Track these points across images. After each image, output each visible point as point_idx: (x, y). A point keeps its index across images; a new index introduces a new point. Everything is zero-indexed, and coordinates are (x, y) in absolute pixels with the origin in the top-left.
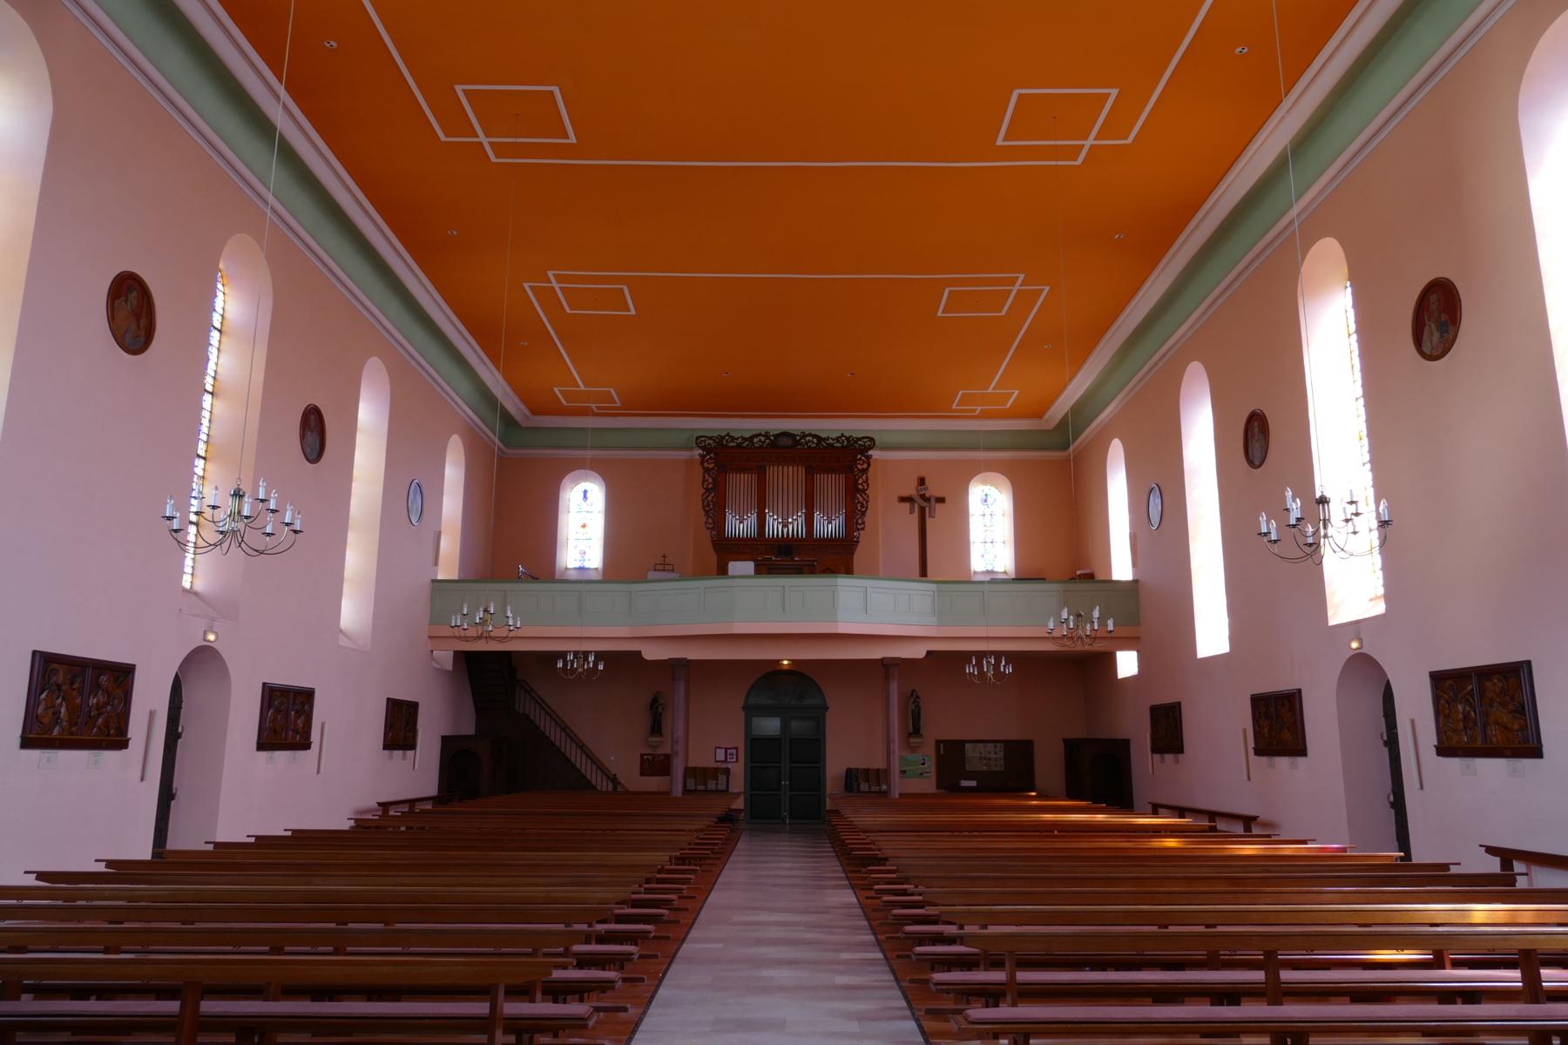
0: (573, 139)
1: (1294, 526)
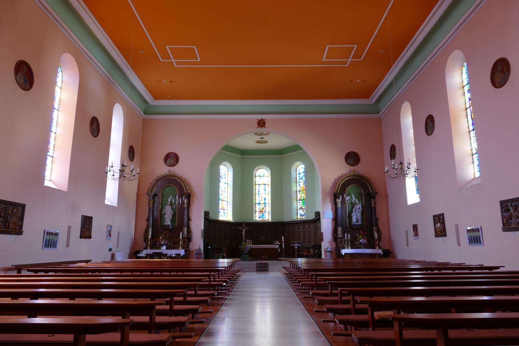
0: (199, 60)
1: (386, 172)
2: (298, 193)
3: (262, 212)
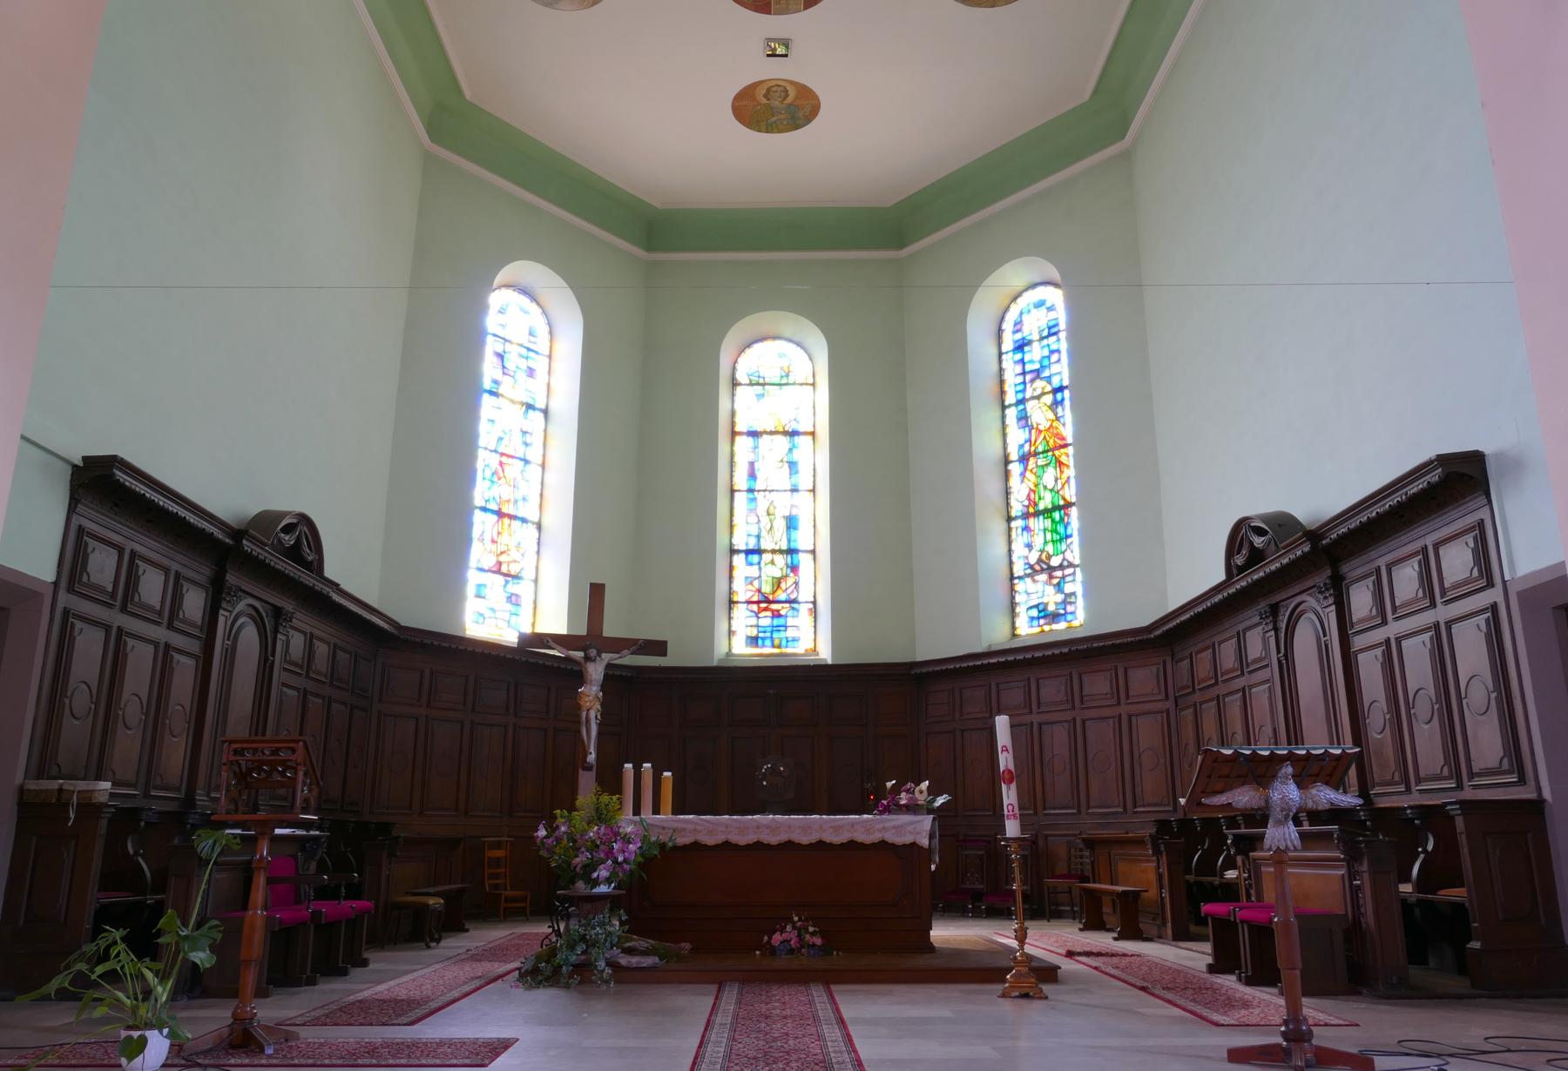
2: (1016, 468)
3: (774, 606)
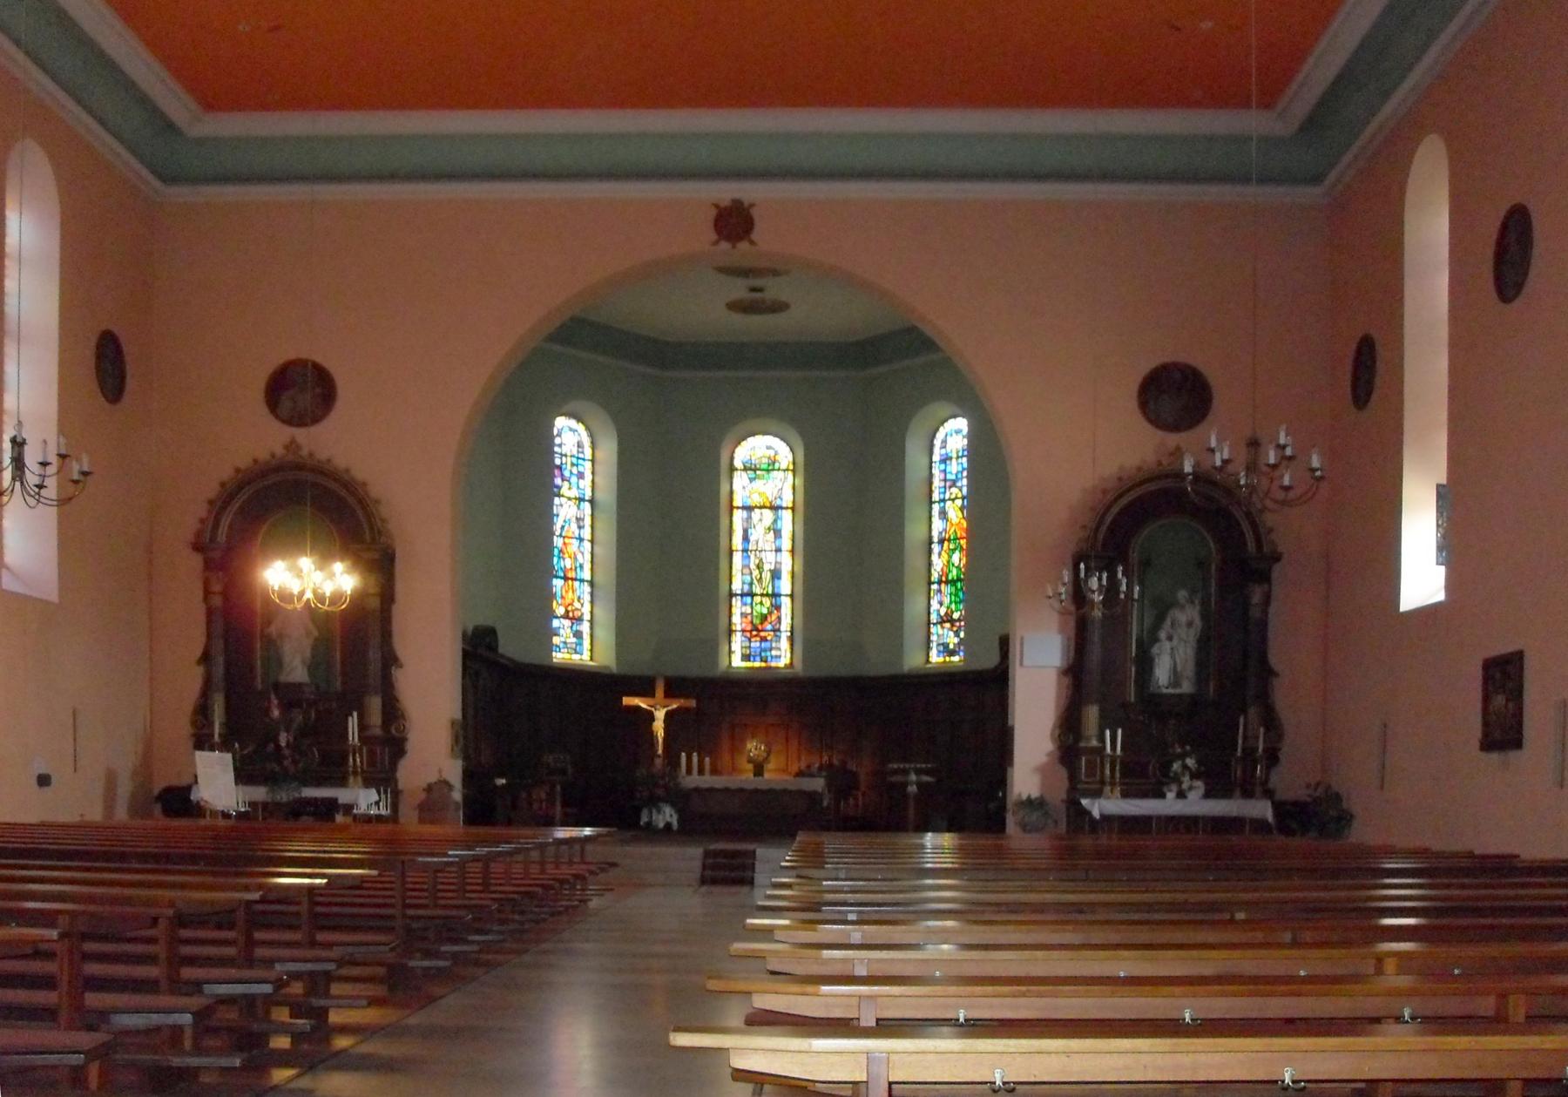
2: (936, 548)
3: (762, 634)
